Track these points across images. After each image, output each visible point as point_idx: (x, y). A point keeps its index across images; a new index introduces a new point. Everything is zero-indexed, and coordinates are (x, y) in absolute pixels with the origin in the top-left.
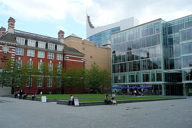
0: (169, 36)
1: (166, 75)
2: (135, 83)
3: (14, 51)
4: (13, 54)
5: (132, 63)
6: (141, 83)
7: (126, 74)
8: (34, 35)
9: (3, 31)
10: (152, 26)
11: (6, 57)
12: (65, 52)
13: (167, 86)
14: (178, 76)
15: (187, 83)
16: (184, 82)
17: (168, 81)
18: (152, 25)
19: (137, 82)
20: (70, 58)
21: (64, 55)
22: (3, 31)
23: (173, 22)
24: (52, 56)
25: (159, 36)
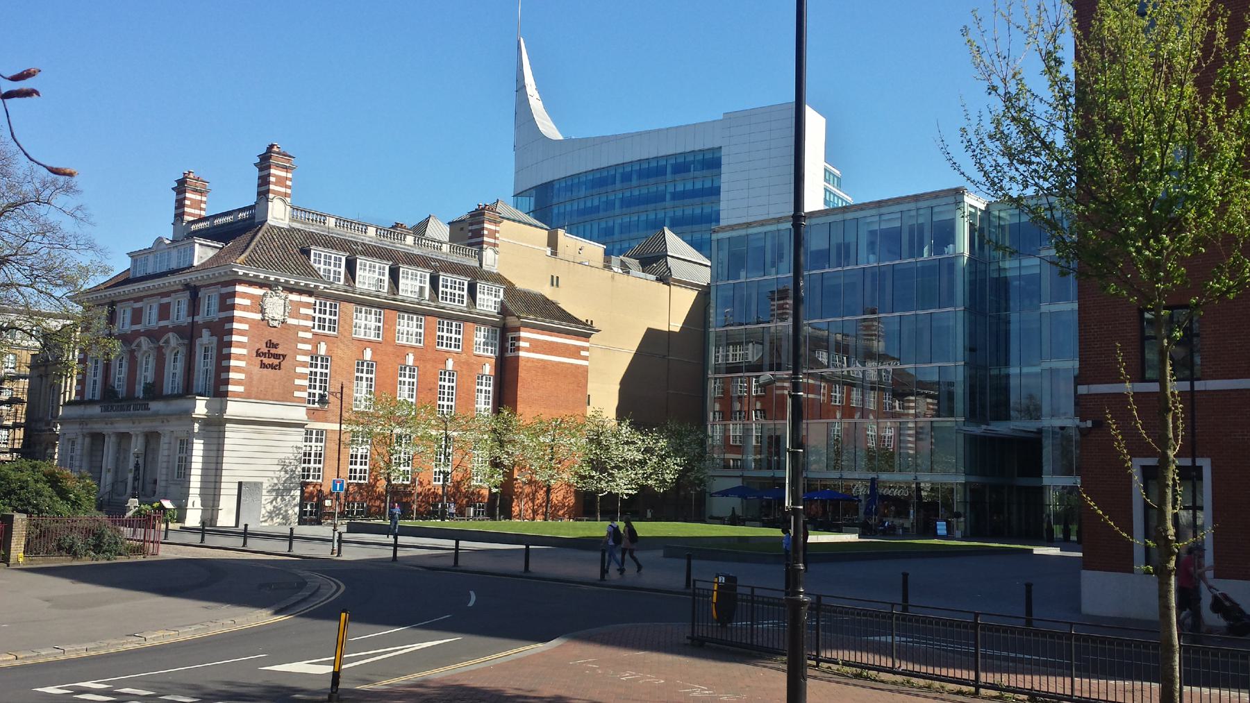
3: (306, 317)
4: (306, 329)
11: (275, 346)
12: (512, 321)
14: (1027, 451)
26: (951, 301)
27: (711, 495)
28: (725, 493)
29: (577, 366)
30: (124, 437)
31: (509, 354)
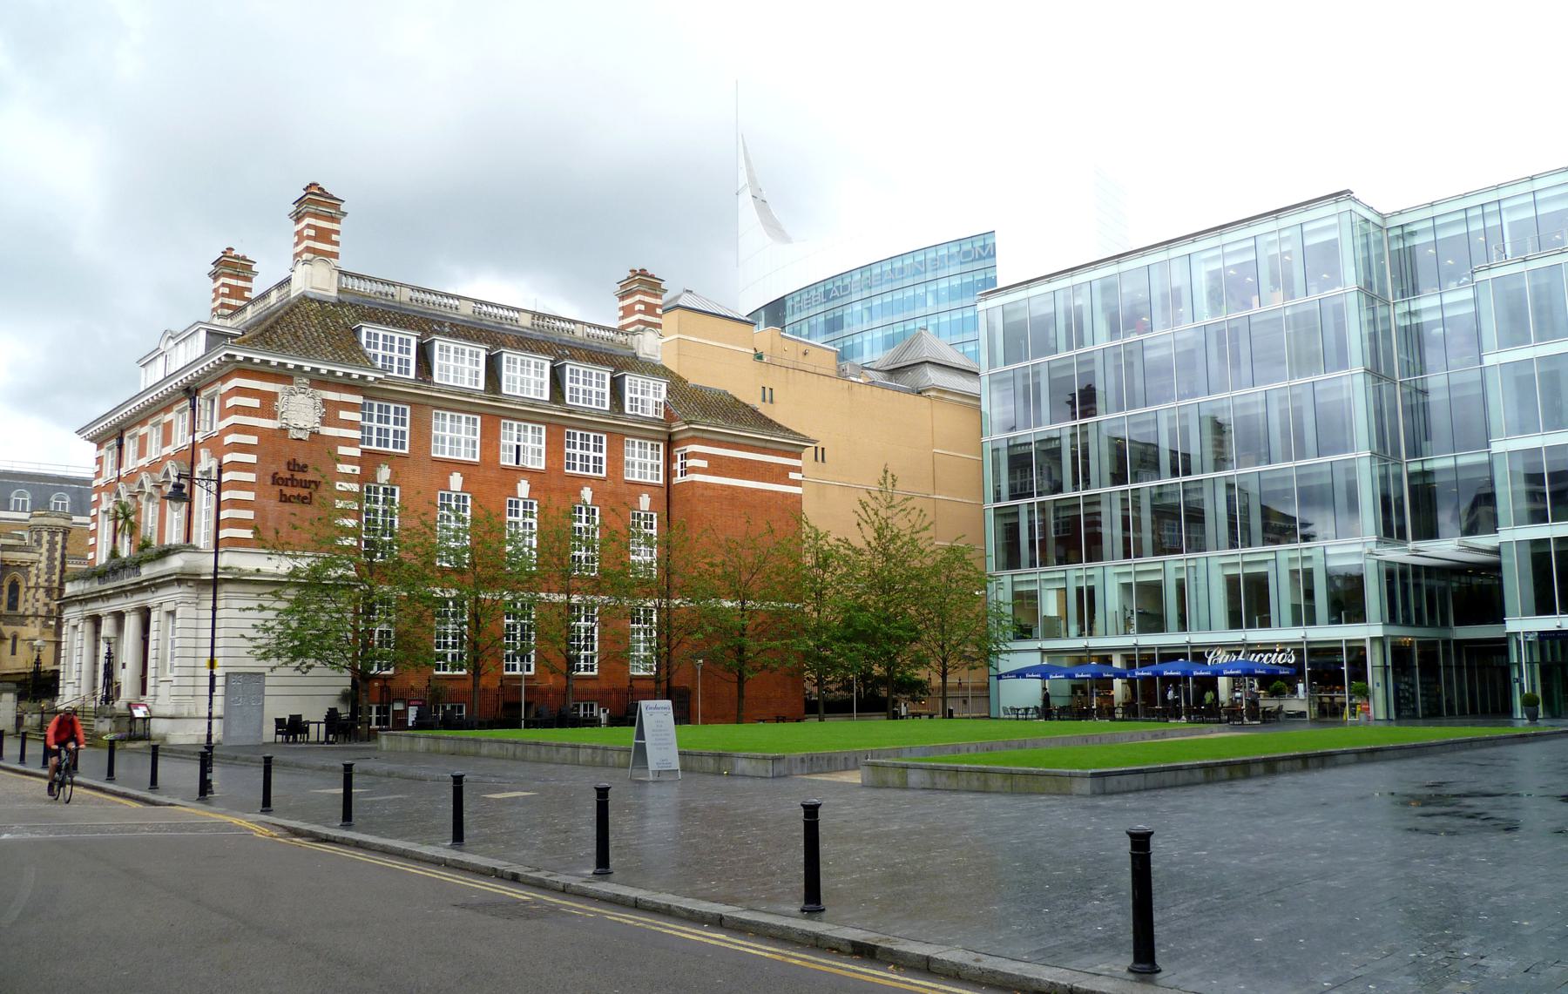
0: (1402, 308)
1: (1394, 576)
2: (1171, 638)
3: (351, 425)
4: (350, 442)
5: (1145, 503)
6: (1213, 632)
7: (1097, 572)
8: (466, 309)
9: (233, 282)
10: (1288, 238)
11: (303, 469)
12: (678, 427)
13: (1400, 656)
15: (1543, 635)
16: (1522, 624)
17: (1407, 622)
18: (1285, 234)
19: (1183, 625)
20: (717, 466)
21: (670, 443)
22: (233, 282)
23: (1429, 213)
24: (592, 454)
25: (1339, 312)
26: (1343, 363)
27: (999, 677)
28: (1020, 674)
29: (785, 495)
30: (119, 617)
31: (678, 479)
